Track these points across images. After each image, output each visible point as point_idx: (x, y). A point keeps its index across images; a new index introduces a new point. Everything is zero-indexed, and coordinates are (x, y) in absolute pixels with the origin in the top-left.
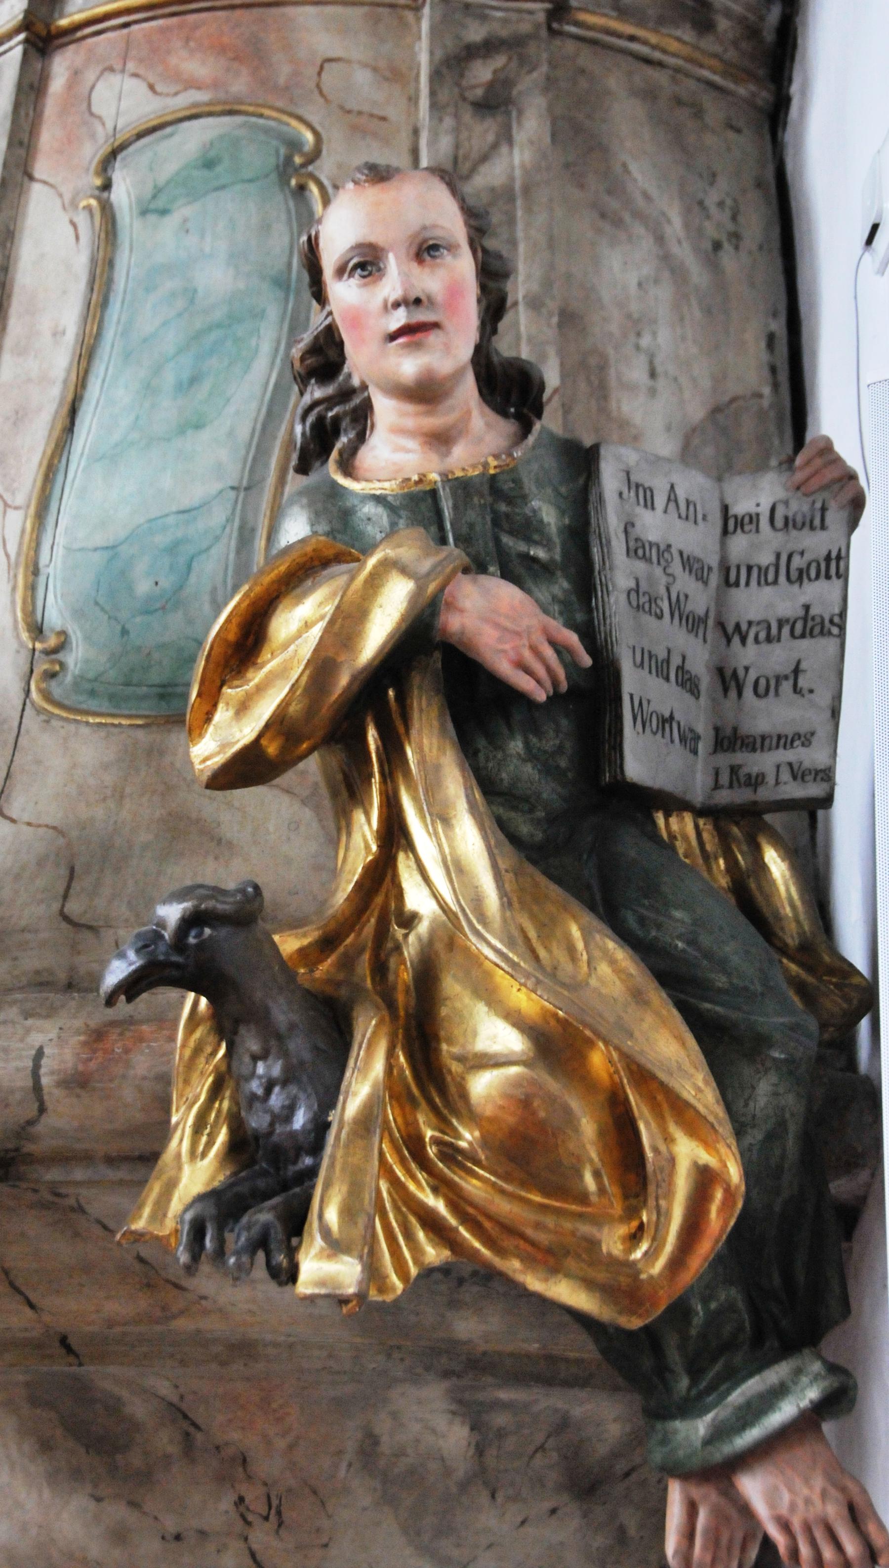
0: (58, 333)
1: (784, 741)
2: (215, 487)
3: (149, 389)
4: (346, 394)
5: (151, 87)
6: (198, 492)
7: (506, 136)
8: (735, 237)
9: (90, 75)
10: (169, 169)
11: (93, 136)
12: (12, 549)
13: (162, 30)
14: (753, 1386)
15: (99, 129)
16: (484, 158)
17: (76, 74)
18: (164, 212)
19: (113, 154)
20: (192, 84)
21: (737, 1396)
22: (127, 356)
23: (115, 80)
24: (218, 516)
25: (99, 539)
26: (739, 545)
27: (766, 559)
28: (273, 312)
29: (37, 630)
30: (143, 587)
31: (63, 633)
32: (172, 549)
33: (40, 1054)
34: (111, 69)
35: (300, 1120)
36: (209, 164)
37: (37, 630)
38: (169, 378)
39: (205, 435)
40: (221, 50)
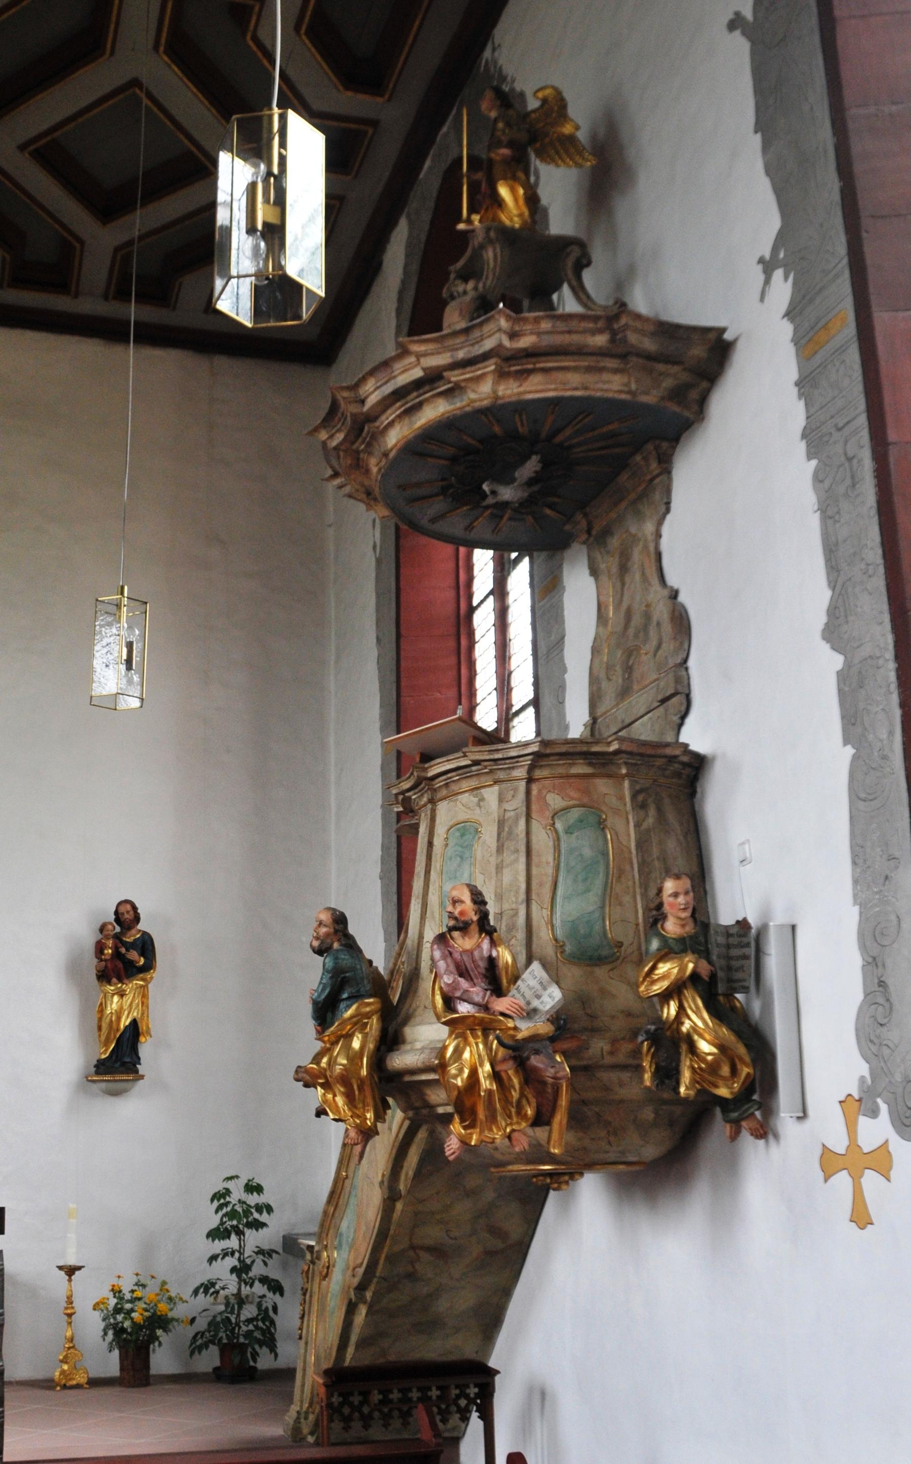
0: (548, 863)
1: (740, 981)
2: (595, 907)
3: (575, 881)
4: (663, 914)
5: (563, 798)
6: (591, 908)
7: (647, 815)
8: (689, 830)
9: (544, 792)
10: (572, 821)
11: (549, 810)
12: (546, 919)
13: (563, 783)
14: (746, 1106)
15: (550, 808)
16: (644, 820)
17: (540, 791)
18: (571, 833)
19: (556, 814)
20: (573, 799)
21: (744, 1109)
22: (568, 871)
23: (553, 795)
24: (597, 915)
25: (569, 919)
26: (731, 940)
27: (736, 943)
28: (602, 861)
29: (556, 940)
30: (582, 932)
31: (563, 942)
32: (588, 922)
33: (602, 1049)
34: (550, 791)
35: (674, 1064)
36: (581, 821)
37: (556, 940)
38: (580, 878)
39: (591, 893)
40: (579, 790)
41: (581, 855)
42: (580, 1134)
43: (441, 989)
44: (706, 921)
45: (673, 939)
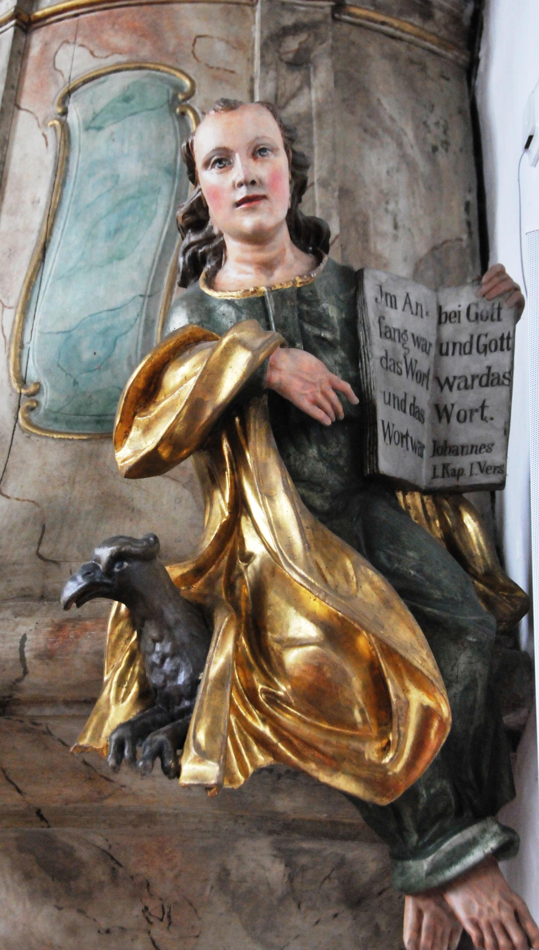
0: (35, 202)
1: (475, 449)
3: (90, 236)
4: (210, 238)
5: (92, 53)
6: (120, 298)
7: (307, 83)
9: (55, 46)
10: (103, 102)
11: (56, 82)
12: (7, 333)
13: (98, 18)
14: (456, 840)
15: (60, 78)
17: (46, 45)
18: (99, 129)
19: (69, 93)
20: (116, 51)
21: (447, 846)
22: (77, 216)
25: (60, 327)
26: (448, 330)
27: (464, 338)
28: (165, 189)
29: (23, 382)
30: (87, 356)
31: (38, 384)
32: (105, 333)
34: (67, 42)
36: (127, 99)
37: (23, 382)
38: (103, 229)
39: (124, 263)
41: (116, 178)
42: (71, 916)
43: (501, 875)
44: (20, 31)
45: (230, 303)
